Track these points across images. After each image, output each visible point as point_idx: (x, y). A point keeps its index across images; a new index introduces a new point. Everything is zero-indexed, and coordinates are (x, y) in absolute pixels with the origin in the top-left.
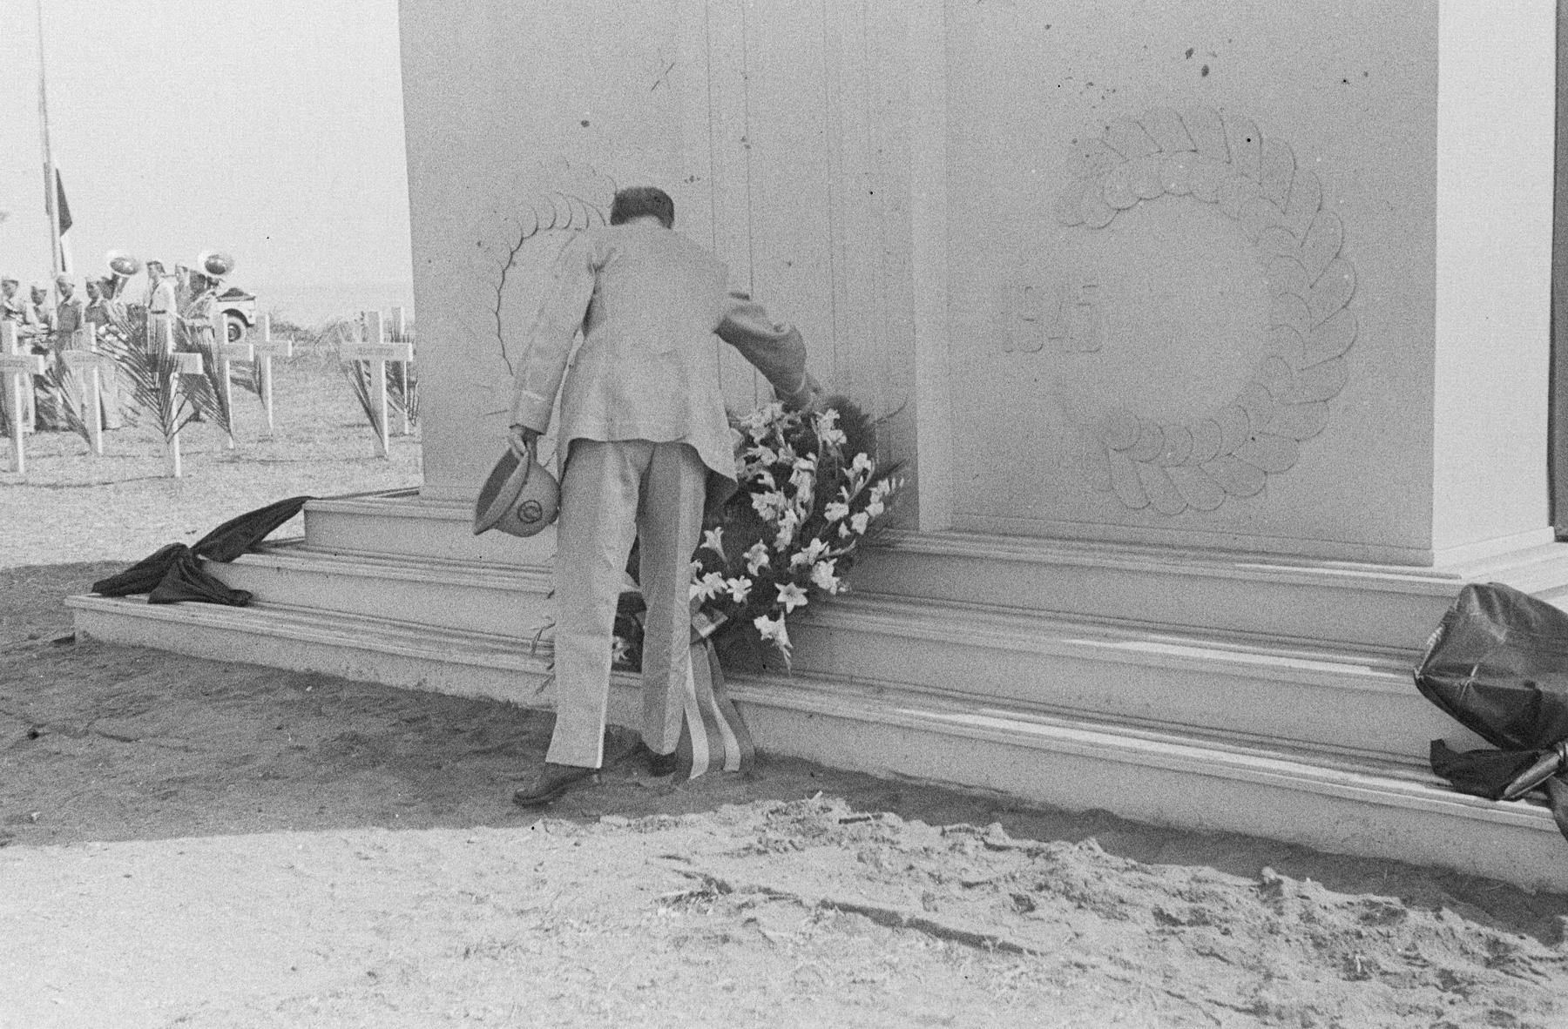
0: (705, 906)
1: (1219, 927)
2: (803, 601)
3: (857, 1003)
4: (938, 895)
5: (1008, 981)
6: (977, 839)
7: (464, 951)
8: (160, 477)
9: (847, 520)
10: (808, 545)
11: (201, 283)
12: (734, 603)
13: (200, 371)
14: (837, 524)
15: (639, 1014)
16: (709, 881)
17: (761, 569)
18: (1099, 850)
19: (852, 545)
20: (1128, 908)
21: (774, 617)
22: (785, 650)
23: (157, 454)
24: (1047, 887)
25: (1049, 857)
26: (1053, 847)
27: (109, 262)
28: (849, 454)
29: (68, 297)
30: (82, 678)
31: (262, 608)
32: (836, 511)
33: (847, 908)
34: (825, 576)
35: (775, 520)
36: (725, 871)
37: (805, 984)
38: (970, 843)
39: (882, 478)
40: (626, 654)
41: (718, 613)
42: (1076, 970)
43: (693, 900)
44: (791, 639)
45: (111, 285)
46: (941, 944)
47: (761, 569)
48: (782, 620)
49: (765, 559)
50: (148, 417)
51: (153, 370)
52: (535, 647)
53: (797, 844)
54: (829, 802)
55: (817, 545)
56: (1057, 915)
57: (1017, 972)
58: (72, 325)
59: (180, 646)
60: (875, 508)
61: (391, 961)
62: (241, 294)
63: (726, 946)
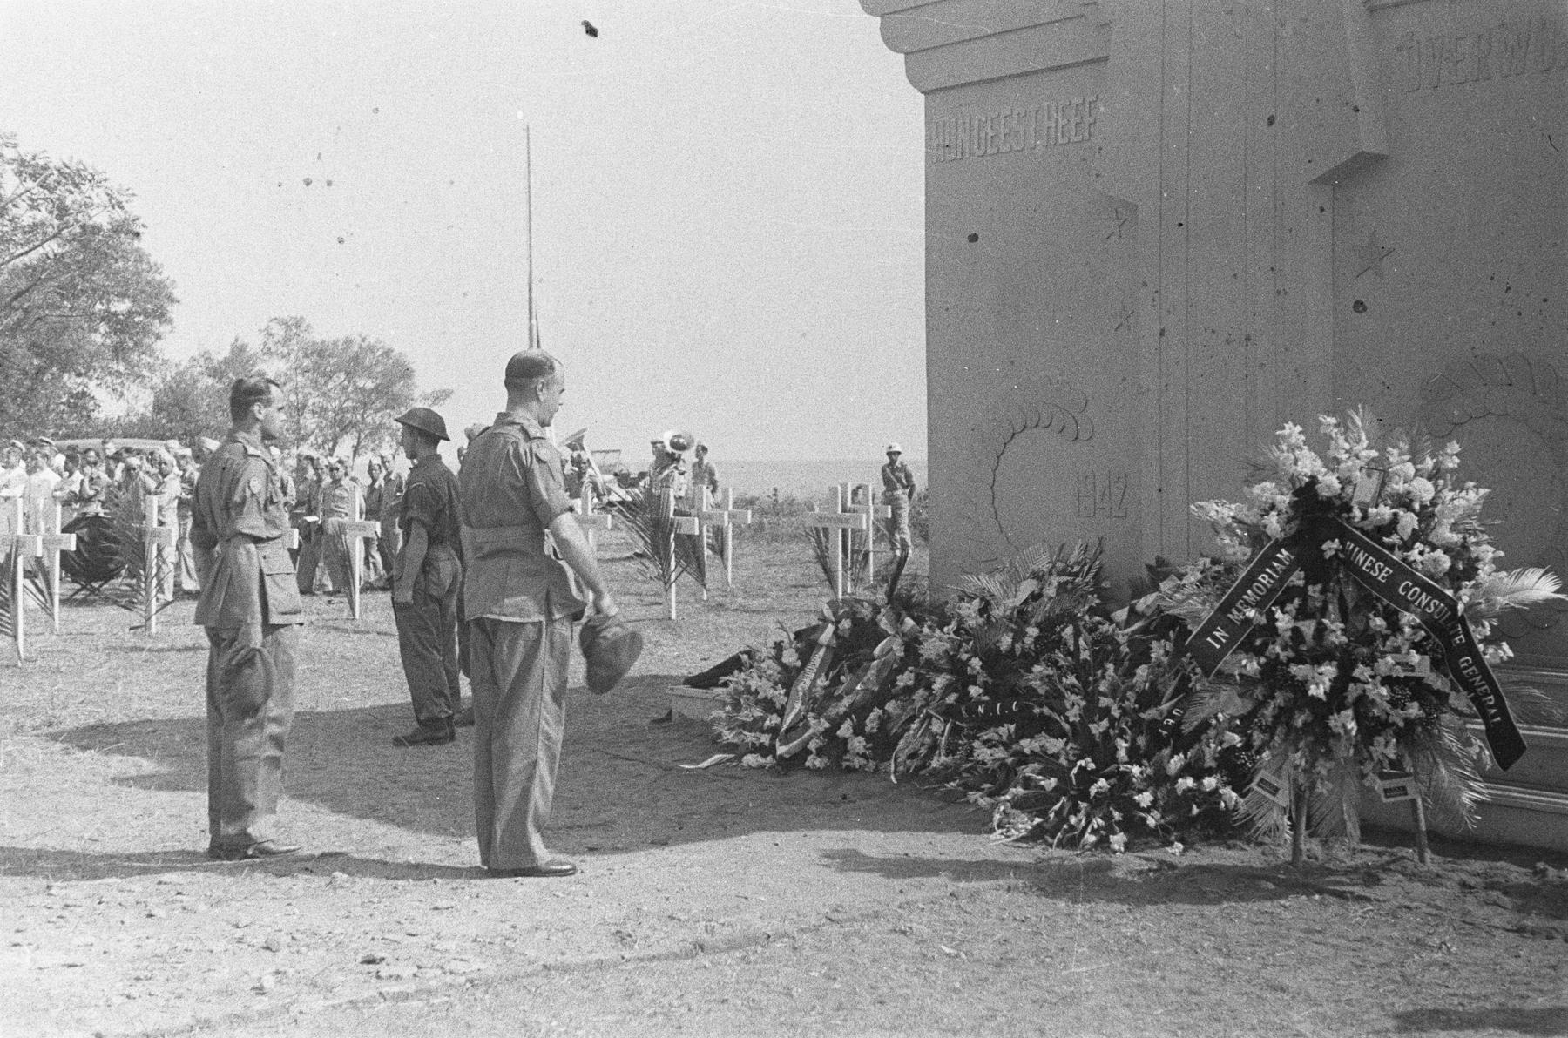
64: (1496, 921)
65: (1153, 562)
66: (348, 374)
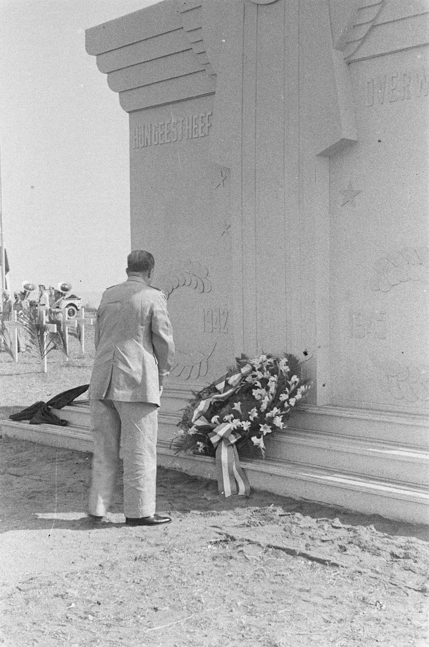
0: (225, 545)
1: (414, 560)
2: (270, 431)
3: (276, 583)
4: (311, 544)
5: (333, 577)
6: (329, 524)
7: (135, 558)
8: (39, 372)
9: (288, 401)
10: (272, 410)
11: (59, 295)
12: (244, 431)
13: (56, 331)
14: (284, 402)
15: (196, 584)
16: (228, 536)
17: (255, 418)
18: (374, 529)
19: (289, 410)
20: (381, 552)
21: (259, 437)
22: (262, 450)
23: (38, 363)
24: (352, 543)
25: (355, 531)
26: (357, 528)
27: (23, 285)
28: (290, 375)
29: (7, 300)
30: (4, 451)
31: (72, 427)
32: (284, 397)
33: (277, 548)
34: (278, 422)
35: (261, 400)
36: (233, 532)
37: (258, 575)
38: (326, 526)
39: (302, 385)
40: (203, 449)
41: (238, 434)
42: (358, 574)
43: (221, 543)
44: (265, 444)
45: (24, 295)
46: (310, 563)
47: (255, 418)
48: (262, 439)
49: (256, 415)
50: (35, 350)
51: (38, 330)
52: (171, 445)
53: (262, 524)
54: (276, 508)
55: (276, 410)
56: (354, 553)
57: (336, 574)
58: (8, 310)
59: (40, 441)
60: (299, 396)
61: (107, 561)
62: (76, 297)
63: (232, 560)
64: (410, 584)
65: (240, 356)
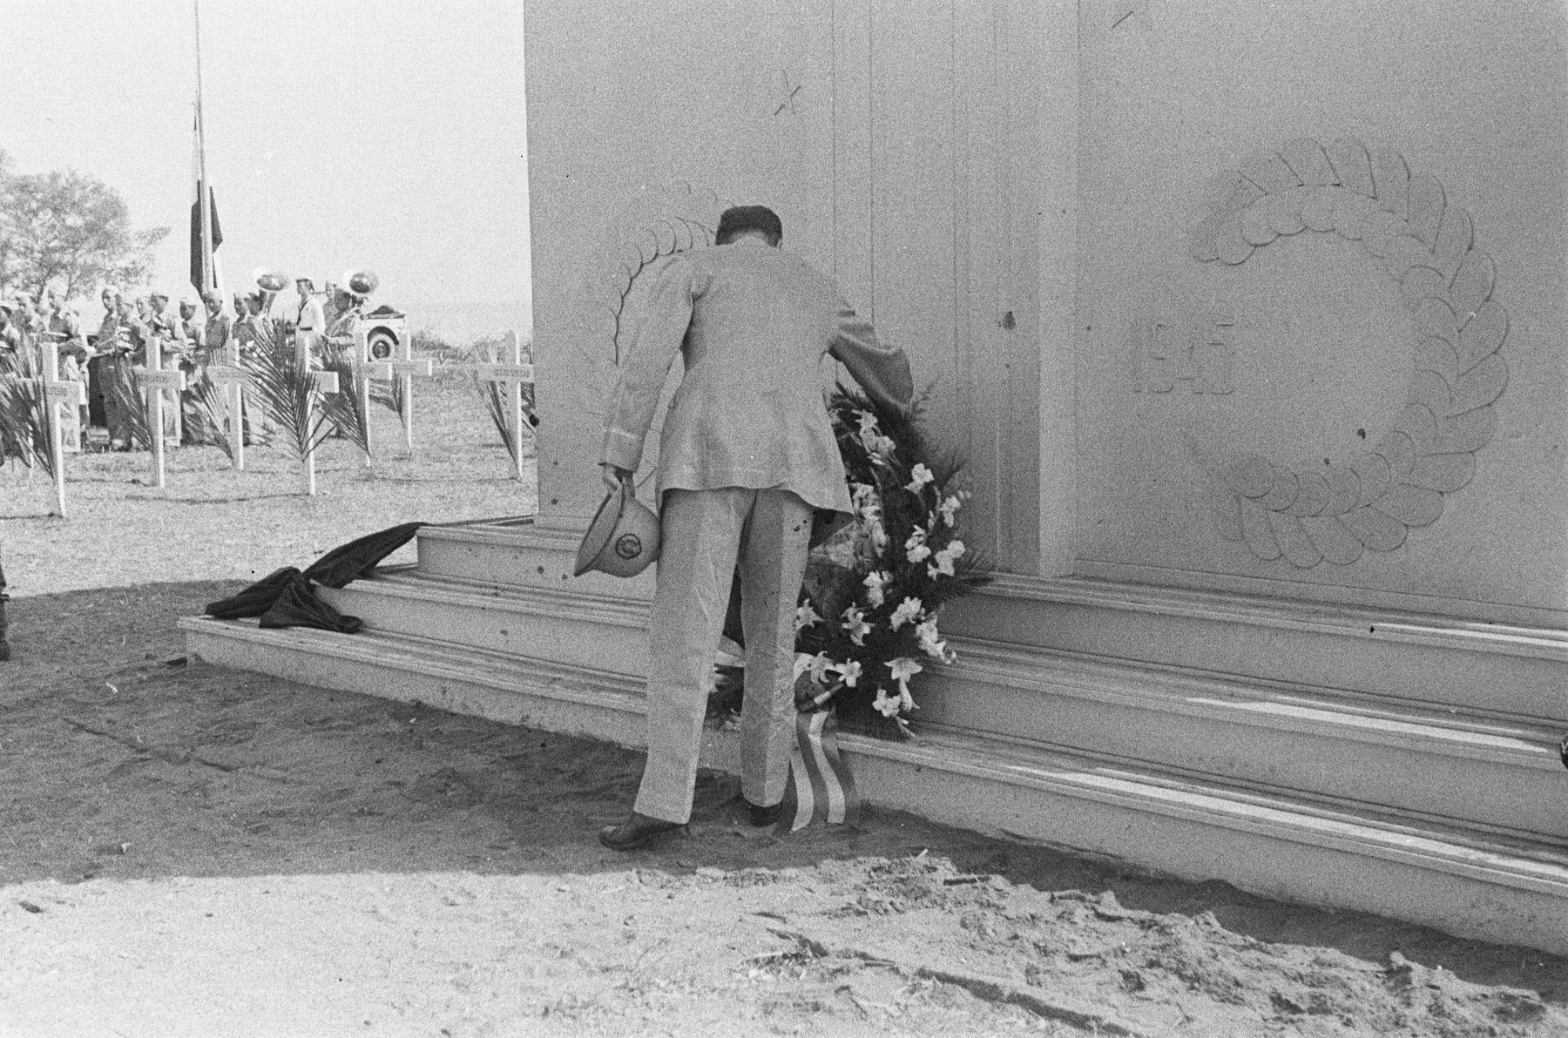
66: (55, 210)
